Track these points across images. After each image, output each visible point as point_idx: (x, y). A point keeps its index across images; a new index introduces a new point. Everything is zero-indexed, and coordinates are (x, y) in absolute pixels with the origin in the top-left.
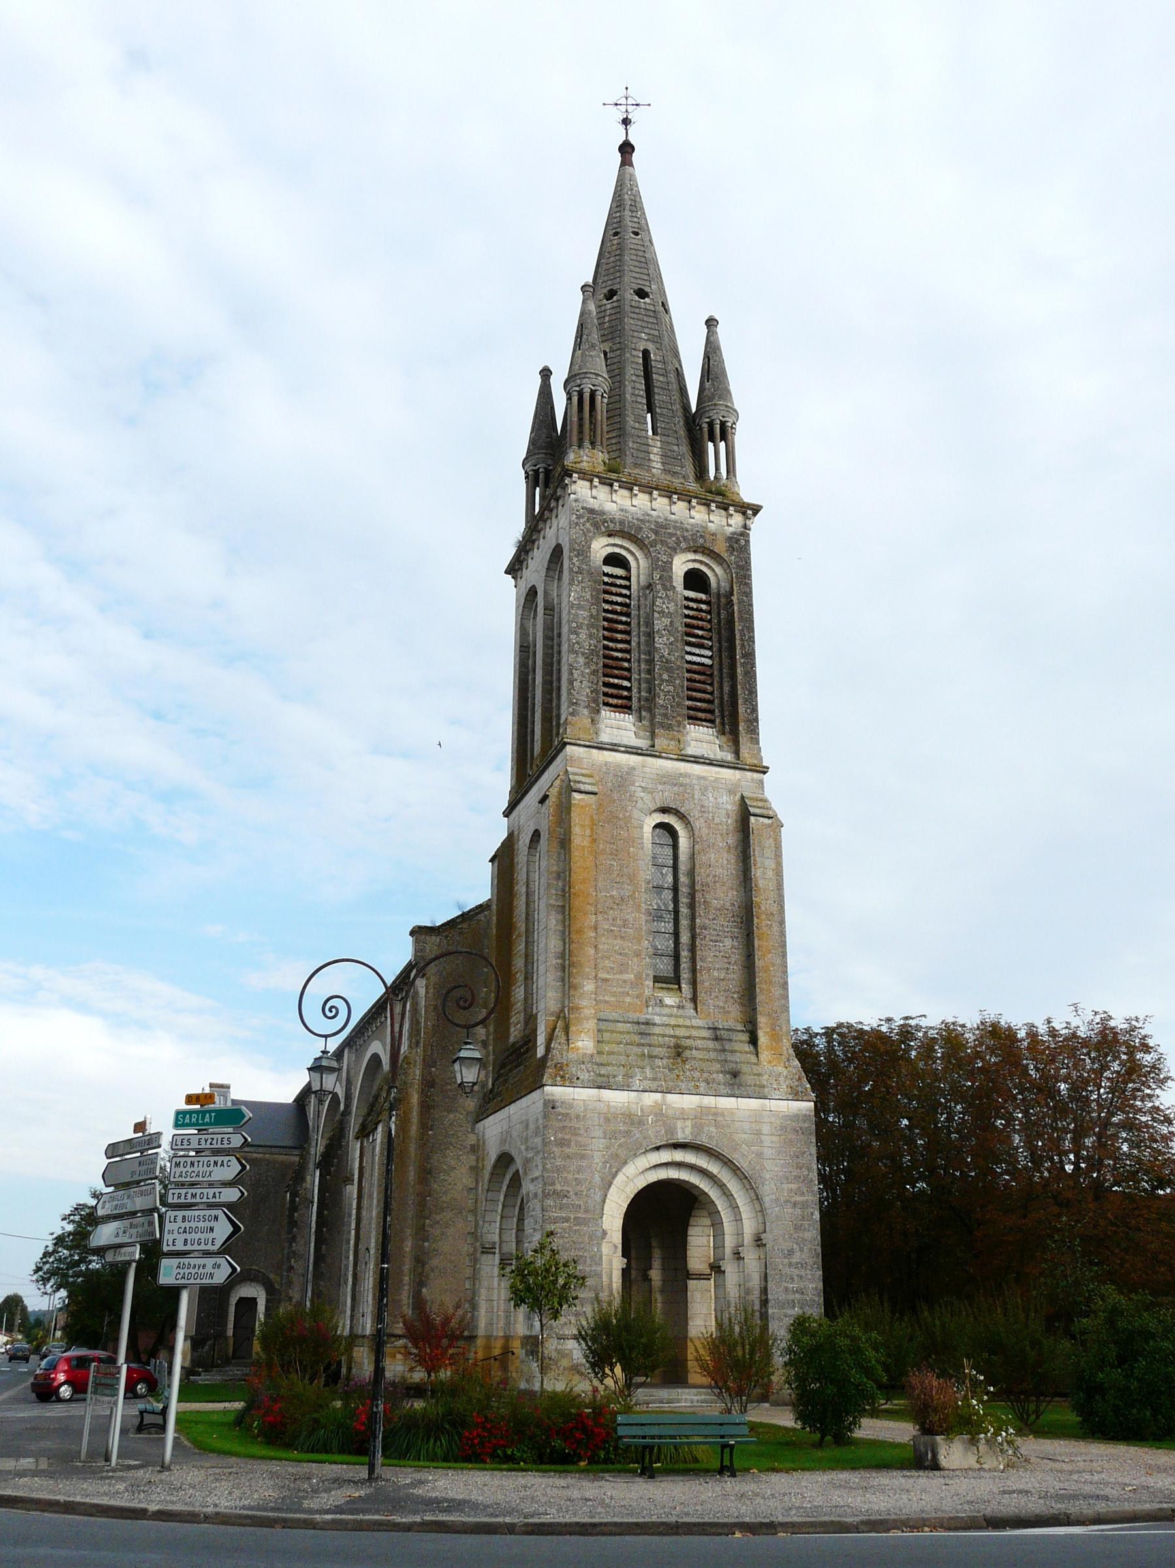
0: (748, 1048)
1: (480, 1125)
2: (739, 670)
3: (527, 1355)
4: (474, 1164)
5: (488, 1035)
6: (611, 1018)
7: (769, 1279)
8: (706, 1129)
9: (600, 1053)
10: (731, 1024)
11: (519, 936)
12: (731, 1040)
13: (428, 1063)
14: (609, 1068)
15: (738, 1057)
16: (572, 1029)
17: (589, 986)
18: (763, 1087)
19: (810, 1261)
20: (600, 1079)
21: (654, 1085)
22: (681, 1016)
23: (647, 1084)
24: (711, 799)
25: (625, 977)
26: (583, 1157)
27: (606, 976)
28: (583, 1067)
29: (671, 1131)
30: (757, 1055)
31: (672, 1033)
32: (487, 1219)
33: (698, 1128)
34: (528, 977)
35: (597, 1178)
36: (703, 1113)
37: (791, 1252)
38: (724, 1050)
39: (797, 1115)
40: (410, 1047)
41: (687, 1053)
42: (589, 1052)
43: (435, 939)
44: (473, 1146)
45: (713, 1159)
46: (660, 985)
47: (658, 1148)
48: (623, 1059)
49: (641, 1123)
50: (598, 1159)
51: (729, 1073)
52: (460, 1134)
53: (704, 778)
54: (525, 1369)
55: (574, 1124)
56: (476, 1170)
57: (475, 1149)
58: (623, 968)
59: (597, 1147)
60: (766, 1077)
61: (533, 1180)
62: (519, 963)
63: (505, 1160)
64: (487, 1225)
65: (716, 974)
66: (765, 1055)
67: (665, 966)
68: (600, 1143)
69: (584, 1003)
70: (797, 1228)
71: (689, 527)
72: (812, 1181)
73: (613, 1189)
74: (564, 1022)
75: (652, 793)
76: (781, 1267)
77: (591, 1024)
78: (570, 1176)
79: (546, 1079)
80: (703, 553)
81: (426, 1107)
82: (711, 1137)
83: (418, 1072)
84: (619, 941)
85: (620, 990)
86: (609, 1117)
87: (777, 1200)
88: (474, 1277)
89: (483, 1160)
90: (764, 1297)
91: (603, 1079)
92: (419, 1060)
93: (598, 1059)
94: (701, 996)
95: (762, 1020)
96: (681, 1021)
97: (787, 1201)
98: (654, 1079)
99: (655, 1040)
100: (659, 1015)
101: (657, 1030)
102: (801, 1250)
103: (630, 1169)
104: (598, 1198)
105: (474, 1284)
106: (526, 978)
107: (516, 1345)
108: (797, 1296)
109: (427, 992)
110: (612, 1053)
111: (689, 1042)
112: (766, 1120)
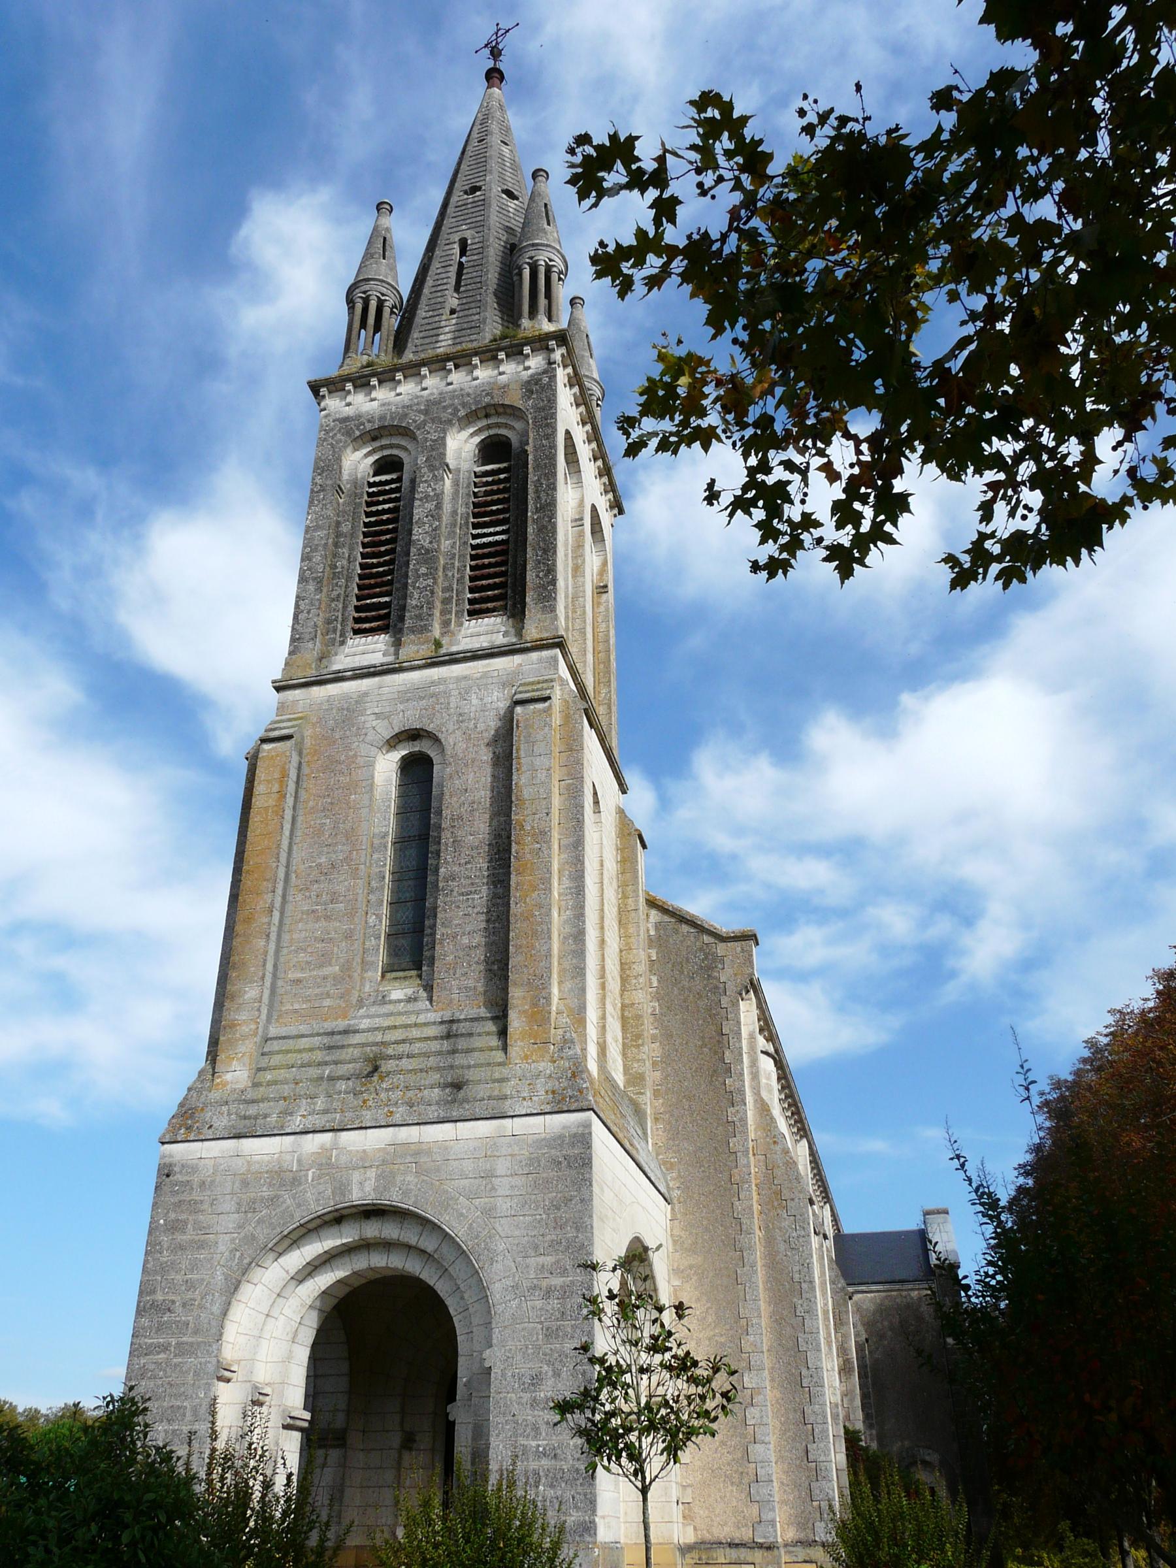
0: (494, 1042)
2: (530, 530)
8: (399, 1178)
9: (256, 1085)
10: (473, 1012)
16: (222, 1057)
23: (309, 1122)
24: (475, 701)
25: (327, 971)
26: (201, 1245)
28: (225, 1109)
29: (342, 1188)
30: (505, 1048)
33: (386, 1180)
35: (219, 1277)
37: (536, 1380)
39: (561, 1137)
42: (241, 1086)
49: (296, 1181)
53: (465, 678)
55: (196, 1196)
68: (230, 1221)
70: (550, 1334)
71: (470, 391)
75: (388, 718)
80: (498, 414)
82: (406, 1193)
84: (323, 923)
85: (317, 991)
87: (515, 1287)
93: (249, 1095)
95: (516, 994)
96: (412, 1019)
97: (535, 1287)
98: (326, 1112)
102: (557, 1374)
104: (216, 1309)
108: (545, 1462)
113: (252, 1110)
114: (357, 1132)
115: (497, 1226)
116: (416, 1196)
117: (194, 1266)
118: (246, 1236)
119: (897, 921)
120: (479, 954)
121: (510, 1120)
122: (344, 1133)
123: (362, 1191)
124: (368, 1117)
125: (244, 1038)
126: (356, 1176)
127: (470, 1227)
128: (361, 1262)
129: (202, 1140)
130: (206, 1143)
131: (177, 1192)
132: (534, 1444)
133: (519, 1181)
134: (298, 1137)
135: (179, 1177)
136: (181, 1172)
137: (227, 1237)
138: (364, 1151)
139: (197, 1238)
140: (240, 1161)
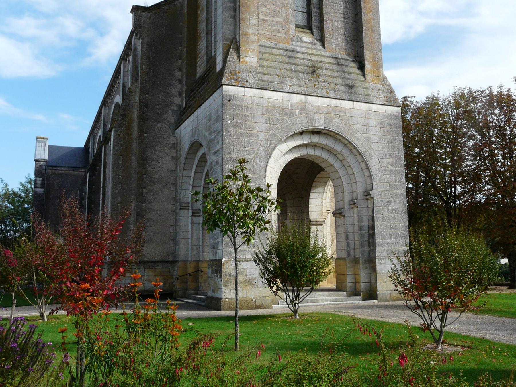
1: (178, 130)
3: (212, 273)
4: (174, 155)
5: (182, 76)
6: (268, 45)
7: (376, 220)
11: (203, 9)
12: (347, 66)
13: (143, 92)
14: (269, 76)
15: (352, 76)
16: (242, 49)
17: (253, 21)
18: (370, 96)
19: (400, 209)
20: (262, 83)
21: (299, 90)
22: (314, 49)
23: (294, 89)
26: (251, 136)
27: (264, 18)
28: (250, 74)
29: (311, 121)
30: (364, 76)
31: (309, 58)
32: (183, 188)
34: (208, 33)
35: (261, 150)
36: (331, 110)
37: (389, 203)
38: (343, 72)
40: (132, 83)
41: (320, 71)
43: (148, 15)
44: (173, 144)
45: (338, 141)
46: (299, 29)
47: (301, 133)
48: (277, 72)
50: (262, 137)
51: (347, 86)
52: (165, 136)
54: (212, 283)
55: (245, 112)
56: (175, 159)
57: (175, 146)
58: (276, 14)
59: (261, 129)
60: (370, 90)
61: (215, 153)
62: (202, 26)
63: (195, 146)
64: (183, 192)
65: (336, 24)
66: (369, 76)
67: (301, 19)
69: (250, 31)
70: (392, 187)
72: (400, 157)
73: (271, 160)
74: (234, 44)
76: (382, 212)
77: (254, 46)
78: (242, 149)
79: (224, 80)
81: (142, 119)
82: (337, 127)
83: (137, 98)
85: (273, 28)
86: (268, 109)
87: (379, 169)
88: (175, 225)
89: (180, 151)
90: (371, 232)
91: (265, 83)
92: (138, 90)
93: (261, 70)
94: (327, 35)
96: (314, 52)
97: (386, 170)
98: (299, 86)
99: (298, 61)
100: (300, 47)
101: (299, 55)
102: (395, 201)
103: (276, 153)
104: (262, 164)
105: (176, 229)
106: (207, 34)
107: (204, 266)
109: (142, 47)
110: (271, 67)
111: (320, 64)
112: (372, 117)
113: (264, 78)
114: (315, 97)
115: (372, 145)
116: (341, 129)
117: (249, 144)
118: (271, 135)
119: (71, 26)
120: (342, 31)
121: (373, 105)
122: (309, 97)
123: (320, 123)
124: (319, 92)
125: (252, 42)
126: (317, 116)
127: (362, 144)
128: (311, 152)
129: (244, 87)
130: (246, 89)
131: (235, 109)
132: (389, 224)
133: (378, 129)
134: (290, 94)
135: (235, 102)
136: (235, 100)
137: (263, 133)
138: (319, 106)
139: (248, 132)
140: (264, 100)
